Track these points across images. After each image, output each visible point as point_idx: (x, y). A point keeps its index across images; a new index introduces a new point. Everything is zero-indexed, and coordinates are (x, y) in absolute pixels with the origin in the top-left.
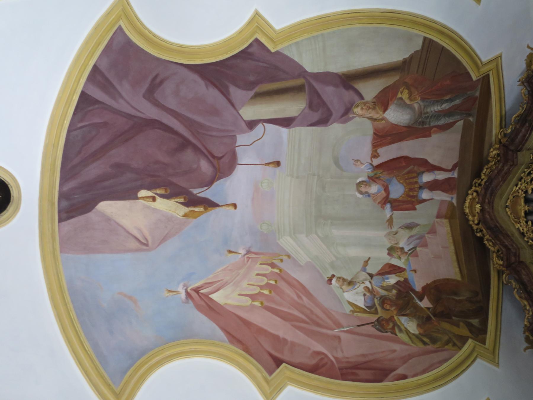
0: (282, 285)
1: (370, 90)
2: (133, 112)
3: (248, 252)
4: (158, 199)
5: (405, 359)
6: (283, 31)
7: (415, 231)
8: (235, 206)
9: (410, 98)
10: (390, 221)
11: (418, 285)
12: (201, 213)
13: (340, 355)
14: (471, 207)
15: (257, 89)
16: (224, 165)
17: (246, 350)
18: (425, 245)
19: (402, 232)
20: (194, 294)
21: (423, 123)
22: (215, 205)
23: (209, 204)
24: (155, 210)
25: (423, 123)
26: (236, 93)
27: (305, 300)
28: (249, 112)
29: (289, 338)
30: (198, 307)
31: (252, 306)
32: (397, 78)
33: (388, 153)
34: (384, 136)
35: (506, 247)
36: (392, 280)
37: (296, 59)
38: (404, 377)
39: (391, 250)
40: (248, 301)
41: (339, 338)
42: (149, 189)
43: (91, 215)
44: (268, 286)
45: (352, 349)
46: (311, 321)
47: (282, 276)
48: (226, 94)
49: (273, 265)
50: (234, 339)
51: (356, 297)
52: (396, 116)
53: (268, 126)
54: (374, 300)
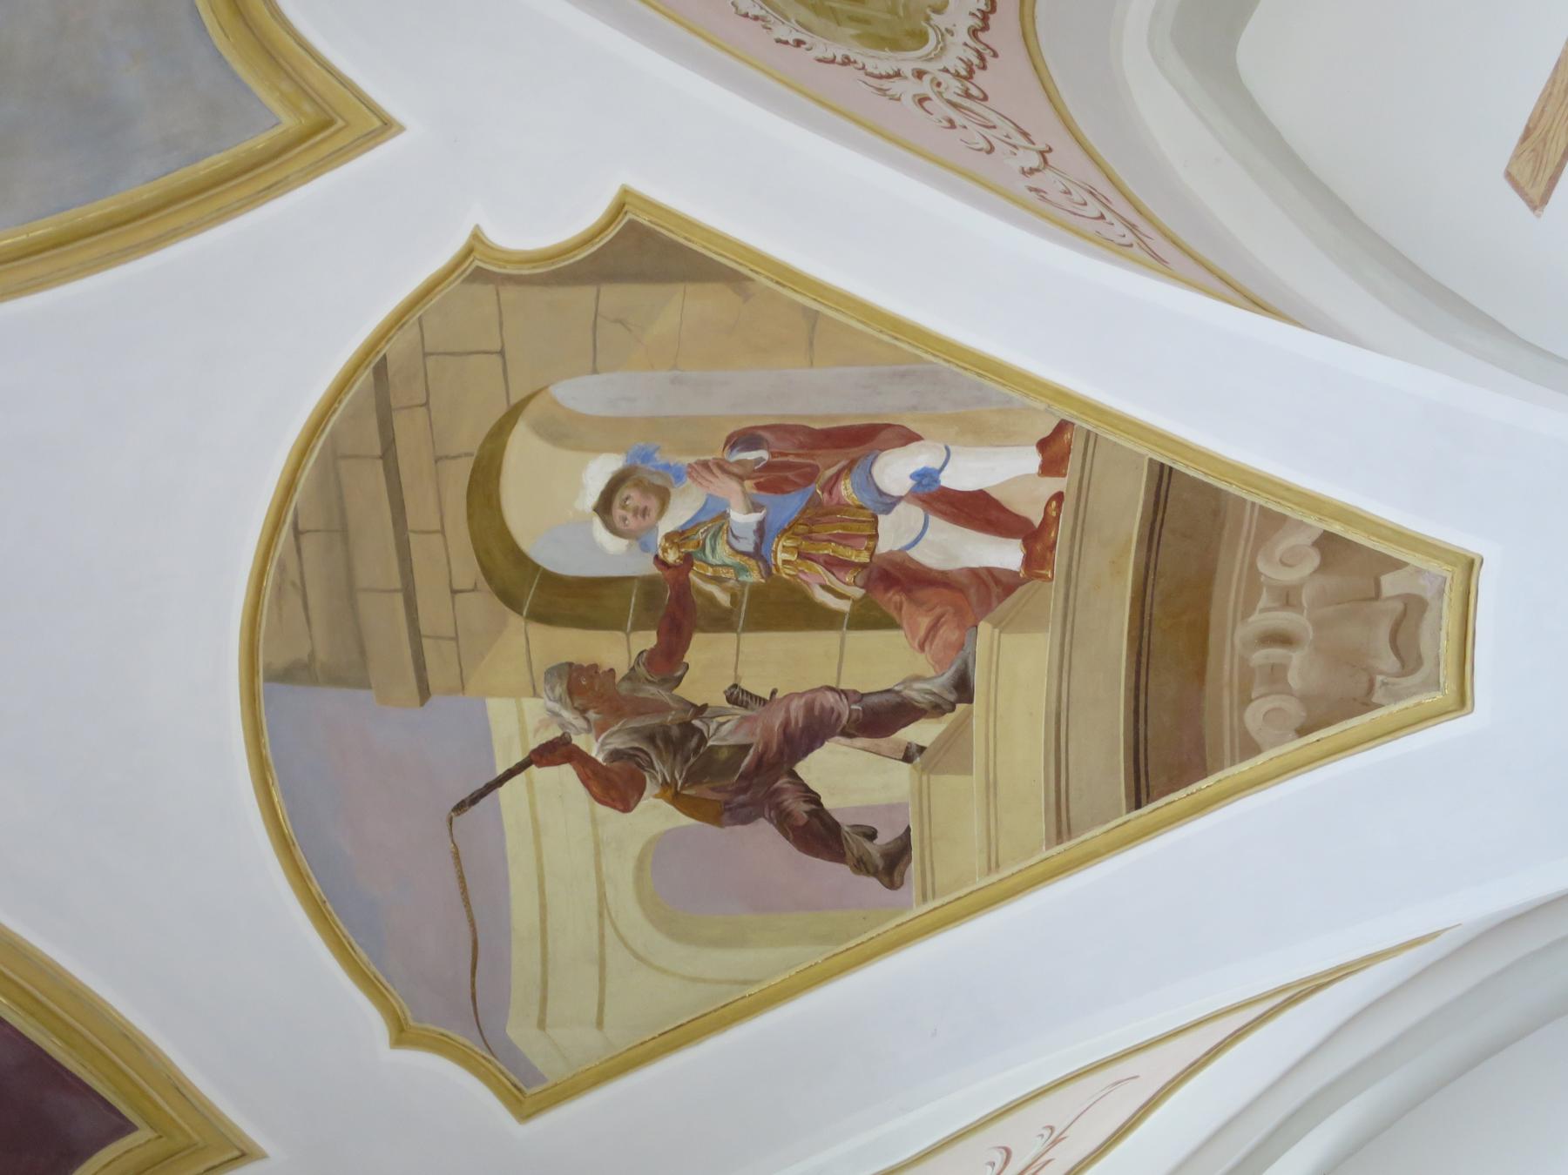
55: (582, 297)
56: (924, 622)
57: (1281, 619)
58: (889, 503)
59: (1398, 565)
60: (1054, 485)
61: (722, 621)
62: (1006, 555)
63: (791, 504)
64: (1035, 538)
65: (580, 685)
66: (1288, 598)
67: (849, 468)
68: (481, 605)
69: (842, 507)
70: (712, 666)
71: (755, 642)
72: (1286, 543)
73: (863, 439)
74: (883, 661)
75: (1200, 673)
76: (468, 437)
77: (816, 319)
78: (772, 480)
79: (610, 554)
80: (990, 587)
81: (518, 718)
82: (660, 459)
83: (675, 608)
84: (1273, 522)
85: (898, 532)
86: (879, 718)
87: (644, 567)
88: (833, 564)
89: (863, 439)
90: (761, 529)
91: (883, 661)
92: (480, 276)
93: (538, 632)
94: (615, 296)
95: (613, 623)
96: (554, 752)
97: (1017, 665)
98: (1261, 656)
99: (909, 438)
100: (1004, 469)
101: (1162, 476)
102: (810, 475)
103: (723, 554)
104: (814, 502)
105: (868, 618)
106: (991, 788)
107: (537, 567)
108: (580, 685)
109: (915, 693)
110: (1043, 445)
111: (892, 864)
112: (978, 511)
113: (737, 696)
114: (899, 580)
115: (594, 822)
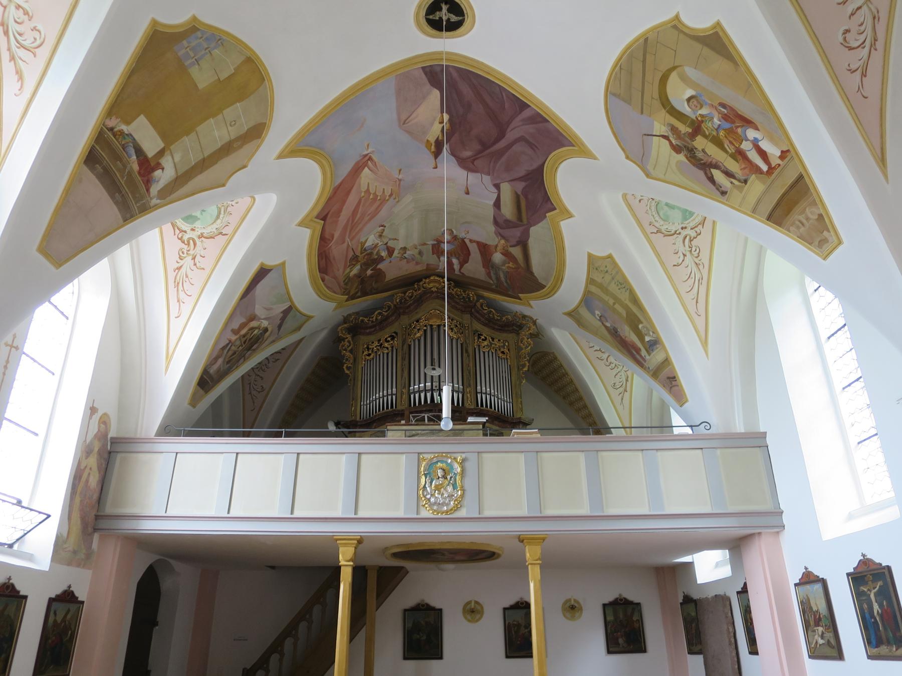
0: (378, 203)
1: (516, 252)
2: (512, 126)
3: (400, 180)
4: (441, 126)
5: (335, 278)
6: (559, 226)
7: (418, 256)
8: (436, 168)
9: (508, 267)
10: (425, 244)
11: (381, 266)
12: (430, 150)
13: (333, 247)
14: (434, 281)
15: (522, 197)
16: (467, 164)
17: (330, 199)
18: (408, 262)
19: (417, 251)
20: (367, 158)
21: (492, 267)
22: (436, 158)
23: (437, 153)
24: (432, 124)
25: (492, 267)
26: (520, 186)
27: (367, 218)
28: (506, 188)
29: (340, 218)
30: (357, 163)
31: (361, 192)
32: (522, 265)
33: (473, 248)
34: (485, 250)
35: (409, 306)
36: (384, 254)
37: (540, 225)
38: (323, 280)
39: (404, 249)
40: (364, 188)
41: (344, 242)
42: (450, 120)
43: (428, 86)
44: (376, 195)
45: (337, 251)
46: (353, 225)
47: (384, 201)
48: (520, 179)
49: (391, 195)
50: (336, 190)
51: (371, 240)
52: (498, 257)
53: (495, 196)
54: (376, 309)
55: (698, 46)
56: (743, 166)
57: (804, 221)
58: (747, 140)
59: (829, 231)
60: (779, 161)
61: (706, 137)
62: (765, 168)
63: (727, 125)
64: (771, 169)
65: (674, 129)
66: (808, 219)
67: (742, 126)
68: (657, 104)
69: (737, 133)
70: (700, 143)
71: (710, 144)
72: (814, 209)
73: (748, 123)
74: (733, 166)
75: (787, 215)
76: (664, 68)
77: (750, 85)
78: (725, 117)
79: (686, 109)
80: (758, 170)
81: (659, 128)
82: (703, 98)
83: (697, 128)
84: (814, 203)
85: (746, 146)
86: (729, 174)
87: (693, 117)
88: (731, 142)
89: (748, 123)
90: (719, 126)
91: (733, 166)
92: (675, 27)
93: (668, 116)
94: (706, 51)
95: (684, 123)
96: (665, 137)
97: (756, 186)
98: (797, 223)
99: (757, 129)
100: (773, 151)
101: (800, 178)
102: (733, 122)
103: (710, 125)
104: (732, 128)
105: (733, 156)
106: (744, 198)
107: (670, 103)
108: (674, 129)
109: (736, 176)
110: (782, 152)
111: (724, 193)
112: (763, 154)
113: (703, 151)
114: (740, 155)
115: (670, 155)
